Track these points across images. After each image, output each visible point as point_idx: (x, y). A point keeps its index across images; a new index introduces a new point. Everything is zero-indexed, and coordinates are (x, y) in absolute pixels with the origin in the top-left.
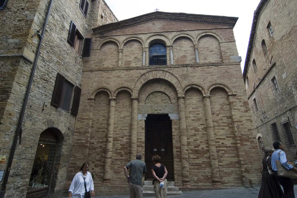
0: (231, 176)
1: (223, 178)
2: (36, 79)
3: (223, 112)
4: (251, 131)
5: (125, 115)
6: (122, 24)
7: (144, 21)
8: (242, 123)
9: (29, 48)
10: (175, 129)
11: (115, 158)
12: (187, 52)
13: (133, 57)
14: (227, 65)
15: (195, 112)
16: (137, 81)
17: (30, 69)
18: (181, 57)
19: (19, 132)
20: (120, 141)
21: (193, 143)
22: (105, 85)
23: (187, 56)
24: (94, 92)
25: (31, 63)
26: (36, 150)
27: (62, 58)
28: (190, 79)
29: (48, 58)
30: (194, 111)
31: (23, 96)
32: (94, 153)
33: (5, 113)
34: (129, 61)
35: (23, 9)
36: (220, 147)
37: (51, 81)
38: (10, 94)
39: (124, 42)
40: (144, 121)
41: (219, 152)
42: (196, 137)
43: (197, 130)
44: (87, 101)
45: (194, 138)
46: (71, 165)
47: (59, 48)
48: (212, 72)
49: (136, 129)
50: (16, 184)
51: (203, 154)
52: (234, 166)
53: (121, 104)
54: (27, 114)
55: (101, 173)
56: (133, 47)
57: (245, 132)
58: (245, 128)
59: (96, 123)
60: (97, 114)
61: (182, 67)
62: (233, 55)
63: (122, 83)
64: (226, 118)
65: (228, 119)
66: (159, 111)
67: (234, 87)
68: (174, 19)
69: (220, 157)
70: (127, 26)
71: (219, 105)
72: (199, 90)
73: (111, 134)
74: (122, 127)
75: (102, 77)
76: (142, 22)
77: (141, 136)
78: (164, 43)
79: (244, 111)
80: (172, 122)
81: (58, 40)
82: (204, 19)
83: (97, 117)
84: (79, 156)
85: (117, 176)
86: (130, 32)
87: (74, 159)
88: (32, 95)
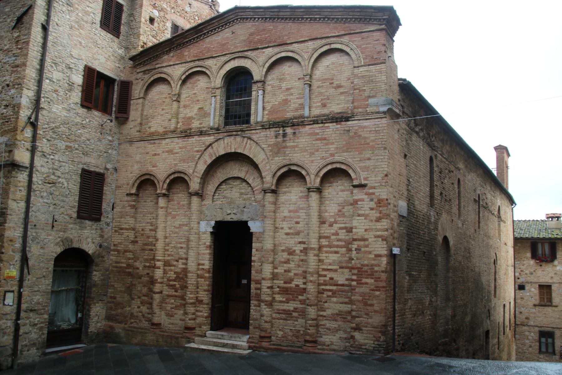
0: (336, 335)
1: (323, 336)
2: (37, 187)
3: (342, 219)
4: (379, 258)
5: (181, 223)
6: (176, 40)
8: (367, 243)
9: (21, 147)
11: (167, 293)
12: (292, 90)
13: (197, 107)
14: (360, 120)
15: (292, 219)
16: (199, 158)
17: (26, 176)
18: (280, 103)
19: (25, 260)
25: (27, 168)
26: (51, 280)
27: (74, 138)
28: (287, 152)
29: (50, 149)
30: (290, 217)
31: (23, 215)
32: (139, 283)
33: (5, 240)
35: (8, 85)
36: (326, 285)
37: (60, 182)
38: (7, 217)
39: (180, 79)
40: (209, 233)
41: (323, 293)
42: (288, 265)
43: (291, 253)
44: (126, 198)
45: (286, 266)
46: (110, 300)
47: (66, 124)
48: (329, 136)
49: (194, 249)
50: (32, 320)
52: (344, 318)
54: (31, 237)
55: (149, 314)
56: (197, 86)
57: (369, 259)
60: (142, 220)
61: (276, 127)
63: (176, 165)
64: (344, 231)
65: (348, 233)
67: (366, 169)
68: (270, 18)
69: (324, 302)
70: (187, 42)
71: (336, 205)
72: (302, 175)
74: (177, 243)
75: (147, 153)
77: (203, 260)
80: (254, 236)
81: (64, 113)
82: (326, 14)
83: (141, 225)
84: (119, 288)
85: (169, 321)
87: (113, 290)
88: (35, 210)
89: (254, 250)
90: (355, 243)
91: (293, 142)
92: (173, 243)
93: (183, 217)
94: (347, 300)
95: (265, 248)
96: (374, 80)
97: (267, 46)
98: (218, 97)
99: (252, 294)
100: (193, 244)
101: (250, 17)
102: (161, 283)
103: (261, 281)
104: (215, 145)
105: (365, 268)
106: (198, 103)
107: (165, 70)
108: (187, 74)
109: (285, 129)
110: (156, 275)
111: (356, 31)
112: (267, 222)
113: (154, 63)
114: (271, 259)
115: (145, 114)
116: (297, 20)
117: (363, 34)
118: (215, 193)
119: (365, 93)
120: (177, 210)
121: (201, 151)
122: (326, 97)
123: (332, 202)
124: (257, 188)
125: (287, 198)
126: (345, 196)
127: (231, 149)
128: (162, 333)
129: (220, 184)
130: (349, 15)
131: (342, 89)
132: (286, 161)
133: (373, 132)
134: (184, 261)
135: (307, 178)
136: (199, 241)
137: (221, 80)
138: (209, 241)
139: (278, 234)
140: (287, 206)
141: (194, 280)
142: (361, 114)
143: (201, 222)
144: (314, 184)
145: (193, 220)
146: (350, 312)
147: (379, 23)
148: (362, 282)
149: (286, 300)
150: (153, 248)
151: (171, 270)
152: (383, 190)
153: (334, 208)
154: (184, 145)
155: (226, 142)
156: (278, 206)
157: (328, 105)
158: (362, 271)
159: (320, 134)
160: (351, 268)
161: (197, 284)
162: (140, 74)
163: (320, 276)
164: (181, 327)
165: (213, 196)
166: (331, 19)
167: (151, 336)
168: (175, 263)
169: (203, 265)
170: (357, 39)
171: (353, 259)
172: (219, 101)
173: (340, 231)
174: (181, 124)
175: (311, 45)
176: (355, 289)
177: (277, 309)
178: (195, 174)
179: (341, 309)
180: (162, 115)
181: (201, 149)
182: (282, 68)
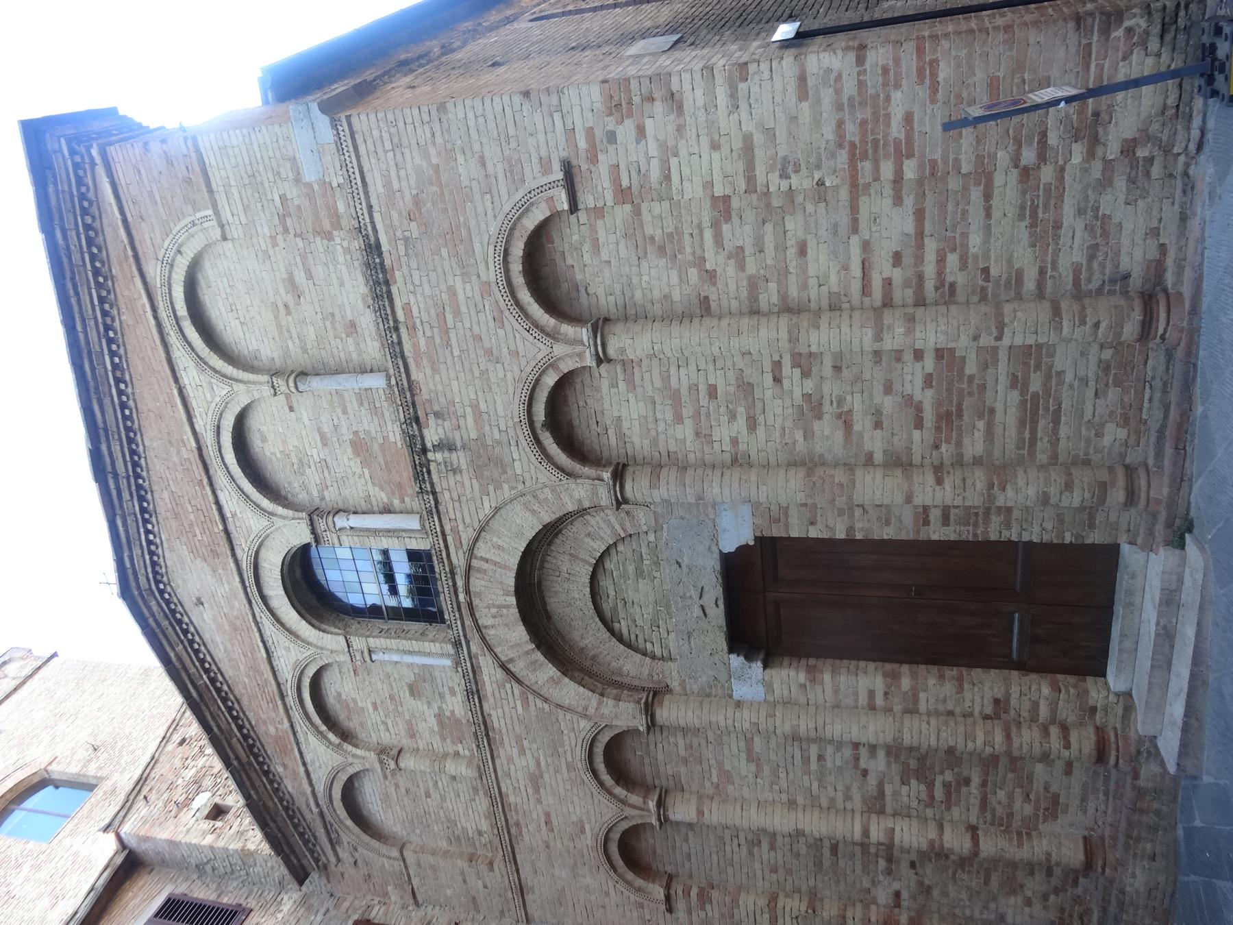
4: (811, 82)
5: (743, 755)
6: (238, 758)
7: (197, 652)
8: (758, 138)
10: (812, 523)
12: (326, 430)
13: (409, 702)
14: (370, 207)
15: (703, 411)
16: (546, 700)
18: (365, 463)
20: (886, 786)
21: (893, 434)
22: (588, 840)
23: (356, 433)
24: (628, 883)
28: (497, 436)
30: (697, 416)
32: (945, 894)
34: (441, 723)
36: (920, 277)
40: (768, 671)
41: (952, 286)
42: (857, 416)
43: (812, 407)
45: (862, 423)
48: (430, 303)
49: (820, 722)
51: (960, 380)
53: (683, 770)
56: (354, 700)
57: (817, 122)
58: (794, 119)
59: (789, 878)
61: (429, 472)
62: (293, 160)
64: (725, 228)
65: (733, 213)
66: (708, 599)
67: (514, 172)
68: (142, 499)
70: (240, 728)
73: (849, 828)
75: (548, 847)
76: (202, 661)
77: (856, 694)
78: (294, 556)
79: (672, 117)
80: (767, 534)
82: (93, 335)
83: (759, 873)
86: (274, 715)
89: (813, 533)
90: (760, 179)
91: (465, 416)
92: (807, 784)
93: (726, 751)
94: (976, 194)
95: (801, 497)
96: (249, 168)
97: (214, 507)
98: (372, 642)
99: (964, 537)
100: (805, 725)
101: (147, 557)
102: (941, 827)
103: (916, 507)
104: (504, 653)
105: (851, 130)
106: (397, 698)
107: (320, 788)
108: (324, 728)
109: (429, 445)
110: (915, 845)
111: (126, 240)
112: (716, 490)
113: (308, 816)
114: (840, 476)
115: (444, 844)
116: (133, 422)
117: (130, 219)
118: (645, 654)
119: (289, 197)
120: (705, 766)
121: (522, 694)
122: (328, 324)
123: (635, 280)
124: (617, 527)
125: (636, 429)
126: (612, 238)
127: (507, 607)
128: (1121, 838)
129: (620, 638)
130: (84, 265)
131: (296, 273)
132: (521, 437)
133: (399, 156)
134: (863, 752)
135: (566, 367)
136: (796, 704)
137: (325, 635)
138: (792, 673)
139: (753, 454)
140: (661, 428)
141: (924, 726)
142: (352, 203)
143: (736, 696)
144: (582, 343)
145: (730, 722)
146: (1026, 174)
147: (87, 166)
148: (902, 136)
149: (981, 416)
150: (827, 844)
151: (896, 794)
152: (575, 100)
153: (653, 272)
154: (514, 744)
155: (489, 622)
156: (664, 454)
157: (349, 317)
158: (863, 141)
159: (429, 334)
160: (856, 189)
161: (937, 713)
162: (341, 856)
163: (888, 303)
164: (1096, 774)
165: (653, 657)
166: (109, 321)
167: (1134, 876)
168: (872, 780)
169: (871, 694)
170: (147, 237)
171: (821, 183)
172: (383, 640)
173: (729, 245)
174: (460, 746)
175: (190, 375)
176: (933, 163)
177: (1018, 448)
178: (591, 711)
179: (1012, 212)
180: (443, 798)
181: (517, 692)
182: (271, 461)
